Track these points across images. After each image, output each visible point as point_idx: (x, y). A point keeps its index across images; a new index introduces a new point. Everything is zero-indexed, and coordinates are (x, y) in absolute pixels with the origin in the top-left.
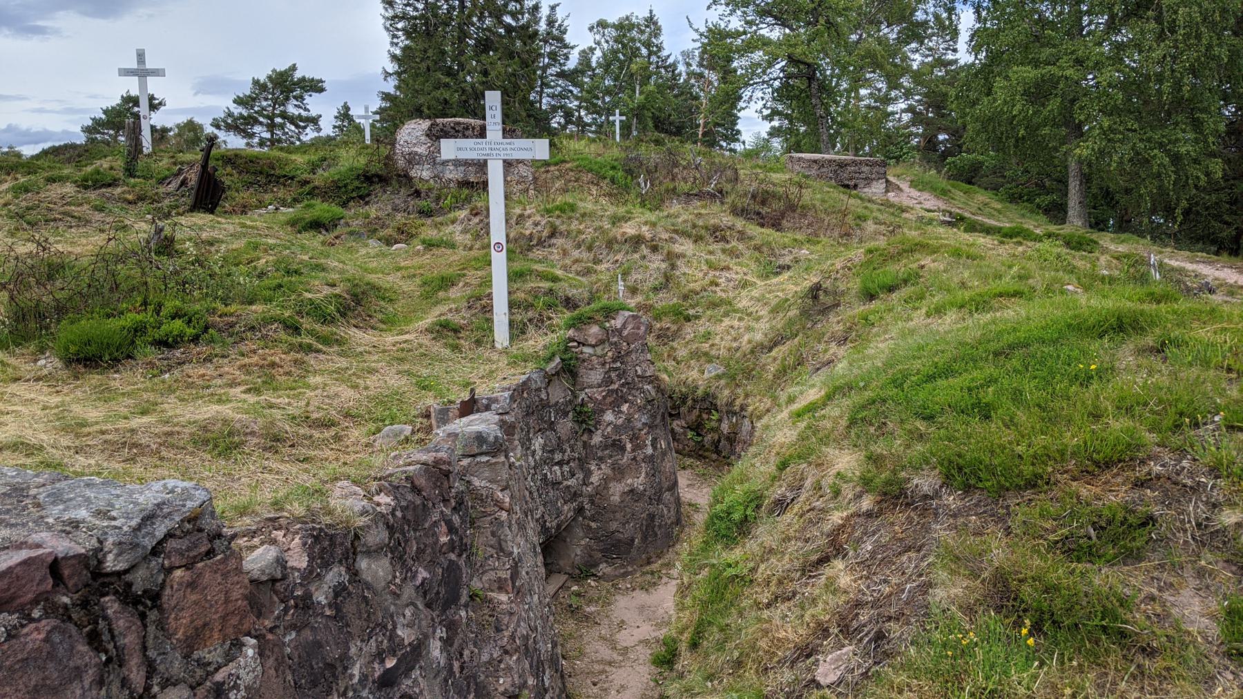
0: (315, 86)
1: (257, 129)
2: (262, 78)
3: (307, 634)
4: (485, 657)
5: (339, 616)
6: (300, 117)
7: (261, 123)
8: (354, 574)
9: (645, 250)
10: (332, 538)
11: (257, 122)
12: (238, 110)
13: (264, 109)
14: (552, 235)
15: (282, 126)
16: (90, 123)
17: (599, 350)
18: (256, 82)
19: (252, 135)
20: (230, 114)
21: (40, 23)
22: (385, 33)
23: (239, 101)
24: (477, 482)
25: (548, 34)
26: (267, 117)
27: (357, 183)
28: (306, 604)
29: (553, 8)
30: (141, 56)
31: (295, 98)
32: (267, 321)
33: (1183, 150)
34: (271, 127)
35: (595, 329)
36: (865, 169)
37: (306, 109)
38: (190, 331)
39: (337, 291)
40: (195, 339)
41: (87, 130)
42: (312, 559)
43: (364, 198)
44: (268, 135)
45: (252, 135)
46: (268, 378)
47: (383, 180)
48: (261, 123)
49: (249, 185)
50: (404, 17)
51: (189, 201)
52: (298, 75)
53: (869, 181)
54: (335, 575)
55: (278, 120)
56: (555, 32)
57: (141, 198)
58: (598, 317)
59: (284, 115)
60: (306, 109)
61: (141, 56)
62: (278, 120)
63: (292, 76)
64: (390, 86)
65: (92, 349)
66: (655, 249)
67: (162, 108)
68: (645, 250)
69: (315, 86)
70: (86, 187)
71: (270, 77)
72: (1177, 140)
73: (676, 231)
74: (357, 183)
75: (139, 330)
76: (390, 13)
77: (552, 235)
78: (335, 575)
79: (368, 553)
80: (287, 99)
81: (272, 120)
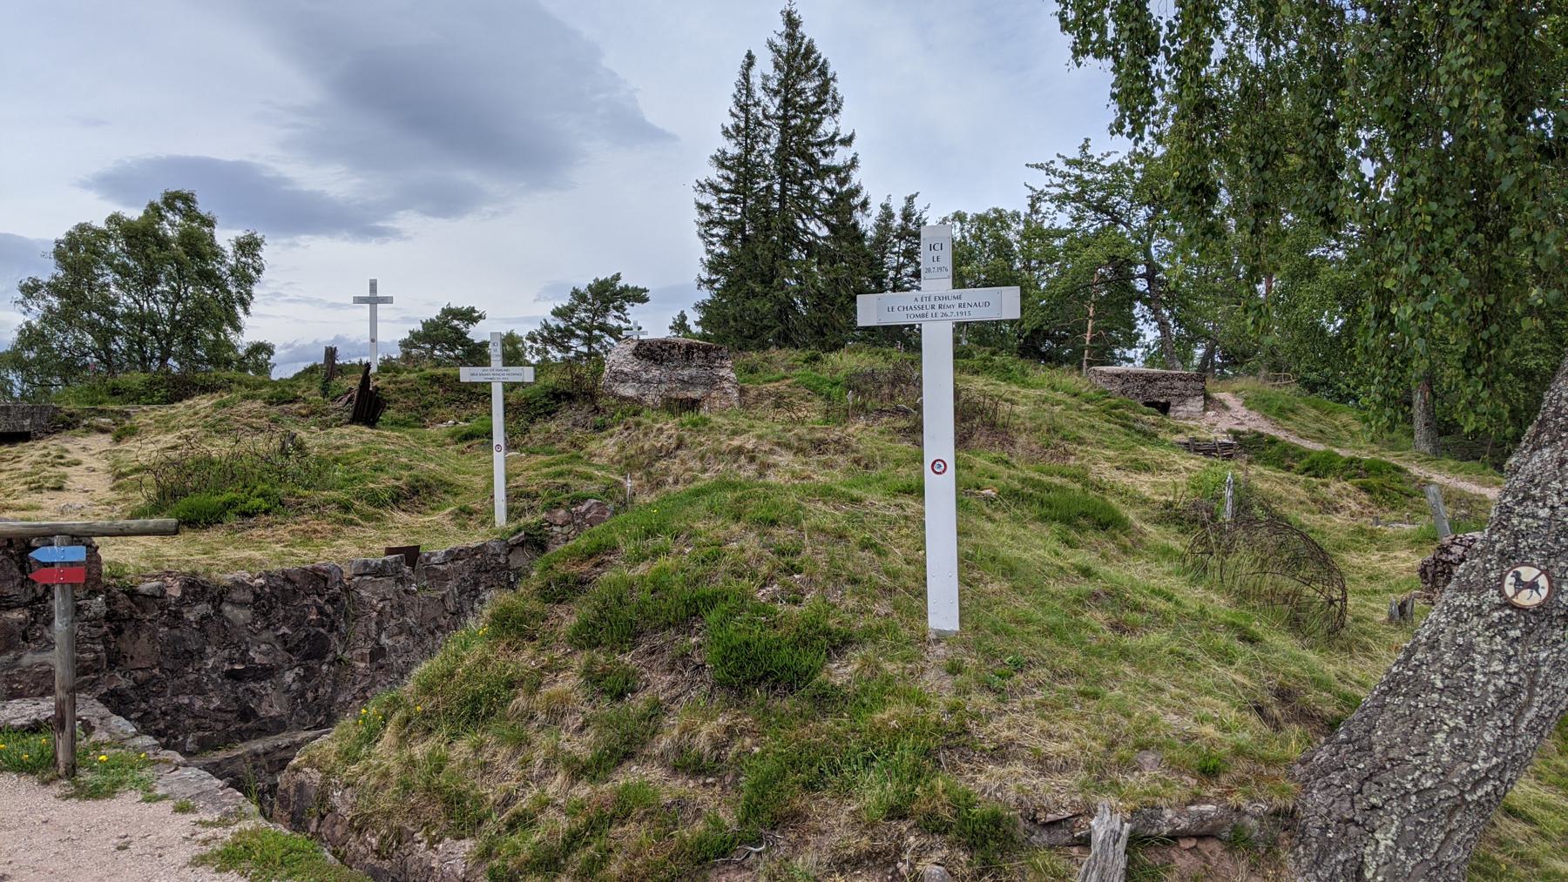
0: (639, 296)
1: (574, 342)
2: (583, 289)
3: (177, 632)
4: (340, 699)
5: (202, 629)
6: (620, 330)
7: (578, 336)
8: (219, 612)
9: (743, 460)
10: (204, 589)
11: (573, 335)
12: (555, 322)
13: (583, 321)
14: (678, 447)
15: (598, 339)
16: (407, 336)
17: (566, 530)
18: (575, 292)
19: (568, 349)
20: (547, 327)
21: (380, 224)
22: (700, 241)
23: (557, 313)
24: (363, 593)
25: (903, 229)
26: (585, 329)
27: (545, 400)
28: (177, 616)
29: (910, 199)
30: (373, 285)
31: (616, 308)
32: (327, 502)
33: (1532, 364)
34: (588, 341)
35: (562, 512)
36: (1179, 384)
37: (627, 321)
38: (265, 506)
39: (399, 483)
40: (267, 512)
41: (404, 344)
42: (184, 593)
43: (550, 414)
44: (585, 349)
45: (568, 349)
46: (307, 537)
47: (570, 397)
48: (578, 336)
49: (451, 402)
50: (721, 222)
51: (349, 415)
52: (621, 284)
53: (1183, 398)
54: (203, 608)
55: (596, 332)
56: (912, 227)
57: (313, 413)
58: (566, 503)
59: (603, 328)
60: (627, 321)
61: (373, 285)
62: (596, 332)
63: (613, 285)
64: (706, 295)
65: (193, 516)
66: (752, 459)
67: (481, 322)
68: (743, 460)
69: (639, 296)
70: (271, 404)
71: (590, 287)
72: (1526, 352)
73: (778, 444)
74: (545, 400)
75: (230, 505)
76: (705, 219)
77: (678, 447)
78: (203, 608)
79: (233, 603)
80: (607, 310)
81: (590, 332)
